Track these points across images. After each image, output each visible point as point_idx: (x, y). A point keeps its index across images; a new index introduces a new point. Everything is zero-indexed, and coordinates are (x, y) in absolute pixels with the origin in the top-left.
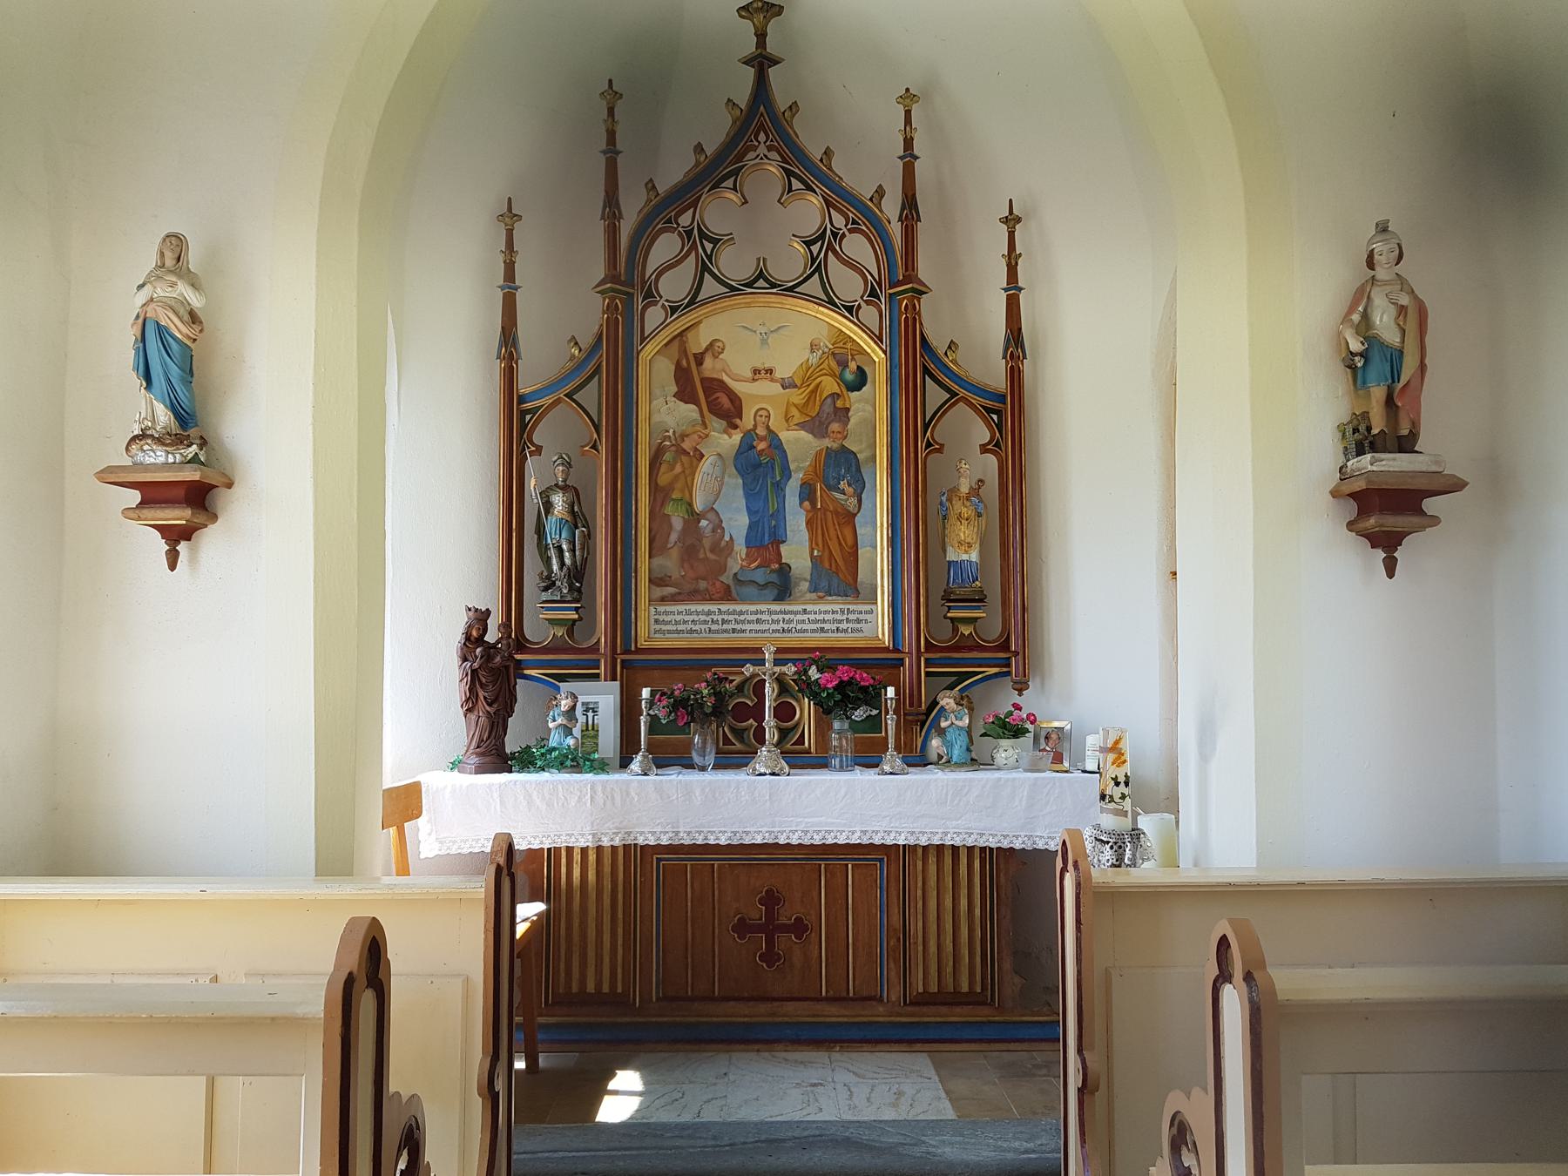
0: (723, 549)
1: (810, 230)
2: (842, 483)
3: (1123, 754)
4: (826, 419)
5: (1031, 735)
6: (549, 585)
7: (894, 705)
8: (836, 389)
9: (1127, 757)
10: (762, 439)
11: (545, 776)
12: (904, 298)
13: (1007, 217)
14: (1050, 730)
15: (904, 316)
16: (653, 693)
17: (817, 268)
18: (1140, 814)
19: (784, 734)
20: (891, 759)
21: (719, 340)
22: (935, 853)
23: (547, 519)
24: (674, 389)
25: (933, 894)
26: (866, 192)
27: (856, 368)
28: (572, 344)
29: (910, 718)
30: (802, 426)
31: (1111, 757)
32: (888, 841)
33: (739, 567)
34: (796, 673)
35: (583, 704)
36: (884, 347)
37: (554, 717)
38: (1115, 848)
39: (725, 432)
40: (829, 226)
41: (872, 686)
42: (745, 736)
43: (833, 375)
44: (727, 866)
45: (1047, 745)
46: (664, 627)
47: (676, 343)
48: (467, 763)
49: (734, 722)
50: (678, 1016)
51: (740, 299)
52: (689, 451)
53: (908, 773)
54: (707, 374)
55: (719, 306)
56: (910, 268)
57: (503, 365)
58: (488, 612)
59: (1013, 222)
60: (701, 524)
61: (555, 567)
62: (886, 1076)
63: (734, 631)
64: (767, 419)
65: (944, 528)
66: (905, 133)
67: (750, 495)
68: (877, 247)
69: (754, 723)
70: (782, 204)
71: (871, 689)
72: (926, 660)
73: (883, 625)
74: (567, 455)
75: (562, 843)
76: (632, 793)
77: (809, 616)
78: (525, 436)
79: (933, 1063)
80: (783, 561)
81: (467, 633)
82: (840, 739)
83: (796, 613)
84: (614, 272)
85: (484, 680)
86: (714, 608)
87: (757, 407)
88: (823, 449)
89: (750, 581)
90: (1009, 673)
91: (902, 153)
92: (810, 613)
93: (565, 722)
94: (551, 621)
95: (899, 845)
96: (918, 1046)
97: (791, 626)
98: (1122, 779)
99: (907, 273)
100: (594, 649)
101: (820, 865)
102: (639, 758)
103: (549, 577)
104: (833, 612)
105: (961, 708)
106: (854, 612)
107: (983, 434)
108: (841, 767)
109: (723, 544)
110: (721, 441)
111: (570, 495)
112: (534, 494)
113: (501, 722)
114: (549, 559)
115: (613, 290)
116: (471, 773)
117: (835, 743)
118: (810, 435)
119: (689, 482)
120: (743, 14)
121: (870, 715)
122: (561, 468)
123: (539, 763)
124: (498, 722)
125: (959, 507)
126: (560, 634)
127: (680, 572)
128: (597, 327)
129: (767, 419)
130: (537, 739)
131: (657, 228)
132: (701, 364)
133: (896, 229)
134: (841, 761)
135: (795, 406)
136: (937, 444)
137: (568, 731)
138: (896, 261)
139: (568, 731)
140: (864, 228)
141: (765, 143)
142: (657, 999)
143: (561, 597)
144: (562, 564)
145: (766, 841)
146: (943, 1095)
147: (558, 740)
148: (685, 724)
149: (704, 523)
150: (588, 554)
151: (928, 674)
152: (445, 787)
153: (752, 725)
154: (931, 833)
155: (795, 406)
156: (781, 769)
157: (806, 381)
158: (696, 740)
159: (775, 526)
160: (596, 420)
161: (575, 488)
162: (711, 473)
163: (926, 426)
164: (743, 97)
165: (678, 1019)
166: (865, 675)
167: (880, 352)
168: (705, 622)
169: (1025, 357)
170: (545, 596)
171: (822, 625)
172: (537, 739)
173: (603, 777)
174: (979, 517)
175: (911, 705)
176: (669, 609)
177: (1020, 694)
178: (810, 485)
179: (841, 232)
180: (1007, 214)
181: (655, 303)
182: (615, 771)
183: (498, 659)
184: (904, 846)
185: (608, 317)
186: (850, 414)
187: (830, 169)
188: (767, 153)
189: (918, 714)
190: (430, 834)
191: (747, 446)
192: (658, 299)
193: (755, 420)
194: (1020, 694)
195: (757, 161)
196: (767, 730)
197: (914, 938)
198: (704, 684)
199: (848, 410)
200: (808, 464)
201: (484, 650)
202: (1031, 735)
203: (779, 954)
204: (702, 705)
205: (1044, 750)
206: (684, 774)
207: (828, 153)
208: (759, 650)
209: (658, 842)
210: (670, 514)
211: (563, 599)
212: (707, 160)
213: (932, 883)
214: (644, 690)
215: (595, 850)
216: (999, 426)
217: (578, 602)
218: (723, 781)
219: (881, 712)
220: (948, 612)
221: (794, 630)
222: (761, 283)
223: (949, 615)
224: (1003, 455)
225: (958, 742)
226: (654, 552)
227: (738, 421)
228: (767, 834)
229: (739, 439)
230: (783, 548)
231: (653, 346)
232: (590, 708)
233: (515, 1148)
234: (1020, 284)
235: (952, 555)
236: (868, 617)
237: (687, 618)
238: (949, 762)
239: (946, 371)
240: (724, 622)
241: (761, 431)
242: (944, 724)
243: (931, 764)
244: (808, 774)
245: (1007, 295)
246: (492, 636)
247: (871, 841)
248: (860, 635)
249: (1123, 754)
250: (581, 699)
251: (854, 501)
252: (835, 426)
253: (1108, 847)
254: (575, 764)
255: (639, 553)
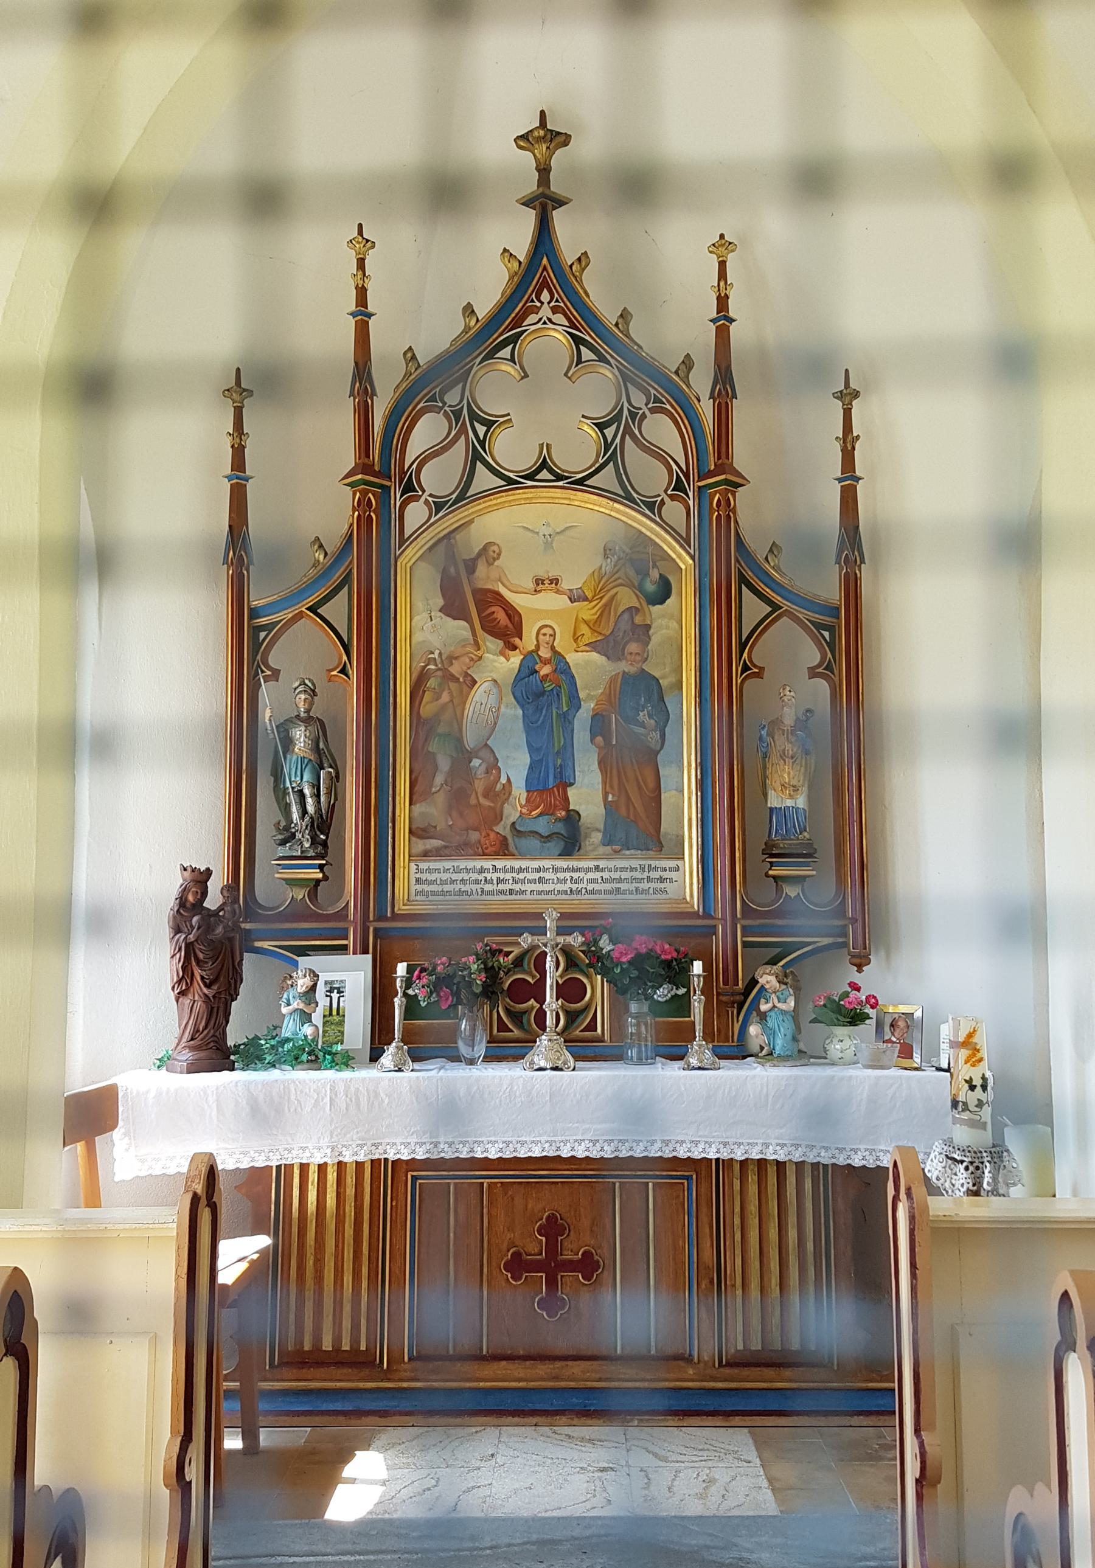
0: (499, 794)
1: (601, 411)
2: (641, 714)
3: (978, 1051)
4: (623, 638)
5: (872, 1022)
6: (288, 837)
7: (701, 984)
8: (634, 602)
9: (984, 1053)
10: (546, 662)
11: (275, 1074)
12: (716, 492)
13: (841, 392)
14: (896, 1016)
15: (716, 513)
16: (410, 970)
17: (610, 455)
18: (1006, 1125)
19: (572, 1017)
20: (699, 1050)
21: (494, 544)
22: (756, 1169)
23: (285, 758)
24: (440, 602)
25: (753, 1222)
26: (672, 364)
27: (658, 576)
28: (316, 547)
29: (724, 999)
30: (593, 646)
31: (964, 1053)
32: (696, 1153)
33: (518, 814)
34: (583, 944)
35: (326, 983)
36: (692, 552)
37: (288, 1000)
38: (971, 1168)
39: (502, 653)
40: (626, 405)
41: (676, 960)
42: (525, 1021)
43: (631, 586)
44: (499, 1185)
45: (893, 1034)
46: (426, 888)
47: (442, 547)
48: (176, 1060)
49: (512, 1004)
50: (436, 1381)
51: (520, 494)
52: (458, 676)
53: (719, 1069)
54: (481, 585)
55: (495, 502)
56: (723, 455)
57: (231, 572)
58: (208, 873)
59: (849, 397)
60: (472, 764)
61: (295, 816)
62: (694, 1458)
63: (511, 892)
64: (552, 638)
65: (765, 768)
66: (719, 290)
67: (531, 726)
68: (684, 430)
69: (535, 1004)
70: (569, 378)
71: (675, 963)
72: (744, 928)
73: (691, 884)
74: (310, 680)
75: (295, 1158)
76: (382, 1095)
77: (601, 874)
78: (259, 657)
79: (755, 1442)
80: (571, 807)
81: (181, 898)
82: (638, 1025)
83: (586, 870)
84: (366, 460)
85: (201, 956)
86: (488, 864)
87: (539, 624)
88: (619, 673)
89: (531, 832)
90: (845, 945)
91: (714, 315)
92: (603, 870)
93: (302, 1006)
94: (292, 882)
95: (711, 1160)
96: (737, 1420)
97: (580, 886)
98: (977, 1082)
99: (720, 461)
100: (342, 915)
101: (614, 1184)
102: (391, 1050)
103: (287, 828)
104: (632, 869)
105: (784, 987)
106: (656, 869)
107: (812, 655)
108: (640, 1059)
109: (499, 787)
110: (496, 664)
111: (314, 728)
112: (269, 728)
113: (222, 1006)
114: (288, 806)
115: (366, 483)
116: (181, 1073)
117: (631, 1030)
118: (604, 657)
119: (458, 713)
120: (522, 144)
121: (676, 994)
122: (303, 696)
123: (268, 1058)
124: (218, 1008)
125: (782, 743)
126: (301, 897)
127: (447, 821)
128: (346, 527)
129: (552, 638)
130: (268, 1027)
131: (419, 407)
132: (474, 572)
133: (706, 410)
134: (639, 1052)
135: (585, 622)
136: (755, 666)
137: (306, 1018)
138: (707, 447)
139: (306, 1018)
140: (668, 407)
141: (549, 303)
142: (410, 1359)
143: (302, 852)
144: (304, 812)
145: (544, 1154)
146: (765, 1483)
147: (293, 1029)
148: (450, 1006)
149: (476, 762)
150: (336, 799)
151: (745, 945)
152: (148, 1092)
153: (533, 1007)
154: (749, 1144)
155: (585, 622)
156: (565, 1063)
157: (598, 593)
158: (463, 1026)
159: (561, 765)
160: (346, 640)
161: (319, 720)
162: (484, 703)
163: (742, 647)
164: (522, 248)
165: (436, 1384)
166: (667, 946)
167: (687, 558)
168: (477, 882)
169: (863, 561)
170: (282, 851)
171: (618, 885)
172: (268, 1027)
173: (347, 1074)
174: (806, 754)
175: (726, 983)
176: (433, 865)
177: (860, 971)
178: (603, 716)
179: (641, 412)
180: (843, 388)
181: (417, 498)
182: (362, 1065)
183: (220, 930)
184: (717, 1160)
185: (359, 516)
186: (651, 632)
187: (628, 336)
188: (551, 316)
189: (733, 994)
190: (127, 1150)
191: (528, 670)
192: (420, 493)
193: (538, 641)
194: (860, 971)
195: (539, 325)
196: (548, 1013)
197: (731, 1280)
198: (472, 958)
199: (648, 627)
200: (600, 691)
201: (202, 919)
202: (872, 1022)
203: (564, 1299)
204: (470, 984)
205: (889, 1041)
206: (446, 1070)
207: (625, 315)
208: (539, 916)
209: (413, 1156)
210: (435, 751)
211: (303, 855)
212: (479, 324)
213: (753, 1208)
214: (399, 964)
215: (335, 1167)
216: (831, 645)
217: (323, 858)
218: (494, 1077)
219: (689, 990)
220: (770, 869)
221: (584, 891)
222: (545, 474)
223: (771, 872)
224: (837, 679)
225: (782, 1029)
226: (414, 798)
227: (517, 641)
228: (547, 1145)
229: (519, 662)
230: (571, 792)
231: (415, 550)
232: (338, 989)
233: (212, 1553)
234: (858, 473)
235: (774, 800)
236: (673, 875)
237: (454, 877)
238: (771, 1054)
239: (766, 580)
240: (499, 881)
241: (545, 653)
242: (764, 1007)
243: (751, 1056)
244: (599, 1069)
245: (842, 486)
246: (213, 901)
247: (674, 1154)
248: (664, 896)
249: (978, 1051)
250: (323, 977)
251: (656, 735)
252: (633, 647)
253: (962, 1167)
254: (313, 1058)
255: (397, 798)
